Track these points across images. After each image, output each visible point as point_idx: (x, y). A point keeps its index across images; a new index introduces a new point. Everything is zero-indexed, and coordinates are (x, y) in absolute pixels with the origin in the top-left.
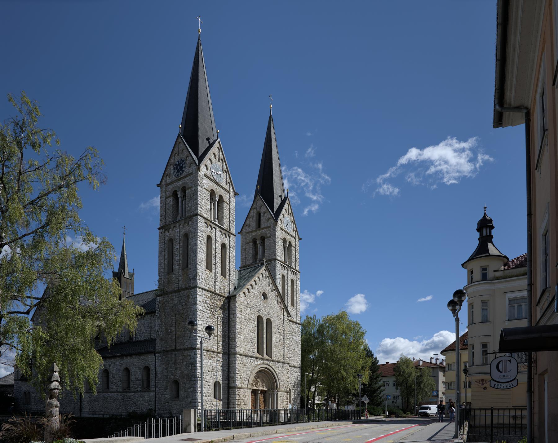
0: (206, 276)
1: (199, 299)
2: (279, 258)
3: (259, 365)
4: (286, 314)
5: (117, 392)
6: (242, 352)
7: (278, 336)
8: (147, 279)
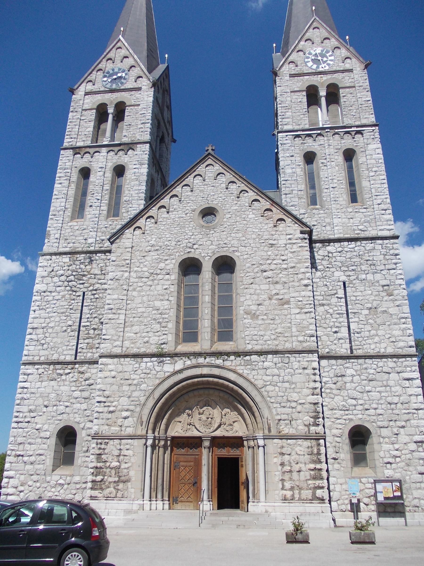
3: (180, 371)
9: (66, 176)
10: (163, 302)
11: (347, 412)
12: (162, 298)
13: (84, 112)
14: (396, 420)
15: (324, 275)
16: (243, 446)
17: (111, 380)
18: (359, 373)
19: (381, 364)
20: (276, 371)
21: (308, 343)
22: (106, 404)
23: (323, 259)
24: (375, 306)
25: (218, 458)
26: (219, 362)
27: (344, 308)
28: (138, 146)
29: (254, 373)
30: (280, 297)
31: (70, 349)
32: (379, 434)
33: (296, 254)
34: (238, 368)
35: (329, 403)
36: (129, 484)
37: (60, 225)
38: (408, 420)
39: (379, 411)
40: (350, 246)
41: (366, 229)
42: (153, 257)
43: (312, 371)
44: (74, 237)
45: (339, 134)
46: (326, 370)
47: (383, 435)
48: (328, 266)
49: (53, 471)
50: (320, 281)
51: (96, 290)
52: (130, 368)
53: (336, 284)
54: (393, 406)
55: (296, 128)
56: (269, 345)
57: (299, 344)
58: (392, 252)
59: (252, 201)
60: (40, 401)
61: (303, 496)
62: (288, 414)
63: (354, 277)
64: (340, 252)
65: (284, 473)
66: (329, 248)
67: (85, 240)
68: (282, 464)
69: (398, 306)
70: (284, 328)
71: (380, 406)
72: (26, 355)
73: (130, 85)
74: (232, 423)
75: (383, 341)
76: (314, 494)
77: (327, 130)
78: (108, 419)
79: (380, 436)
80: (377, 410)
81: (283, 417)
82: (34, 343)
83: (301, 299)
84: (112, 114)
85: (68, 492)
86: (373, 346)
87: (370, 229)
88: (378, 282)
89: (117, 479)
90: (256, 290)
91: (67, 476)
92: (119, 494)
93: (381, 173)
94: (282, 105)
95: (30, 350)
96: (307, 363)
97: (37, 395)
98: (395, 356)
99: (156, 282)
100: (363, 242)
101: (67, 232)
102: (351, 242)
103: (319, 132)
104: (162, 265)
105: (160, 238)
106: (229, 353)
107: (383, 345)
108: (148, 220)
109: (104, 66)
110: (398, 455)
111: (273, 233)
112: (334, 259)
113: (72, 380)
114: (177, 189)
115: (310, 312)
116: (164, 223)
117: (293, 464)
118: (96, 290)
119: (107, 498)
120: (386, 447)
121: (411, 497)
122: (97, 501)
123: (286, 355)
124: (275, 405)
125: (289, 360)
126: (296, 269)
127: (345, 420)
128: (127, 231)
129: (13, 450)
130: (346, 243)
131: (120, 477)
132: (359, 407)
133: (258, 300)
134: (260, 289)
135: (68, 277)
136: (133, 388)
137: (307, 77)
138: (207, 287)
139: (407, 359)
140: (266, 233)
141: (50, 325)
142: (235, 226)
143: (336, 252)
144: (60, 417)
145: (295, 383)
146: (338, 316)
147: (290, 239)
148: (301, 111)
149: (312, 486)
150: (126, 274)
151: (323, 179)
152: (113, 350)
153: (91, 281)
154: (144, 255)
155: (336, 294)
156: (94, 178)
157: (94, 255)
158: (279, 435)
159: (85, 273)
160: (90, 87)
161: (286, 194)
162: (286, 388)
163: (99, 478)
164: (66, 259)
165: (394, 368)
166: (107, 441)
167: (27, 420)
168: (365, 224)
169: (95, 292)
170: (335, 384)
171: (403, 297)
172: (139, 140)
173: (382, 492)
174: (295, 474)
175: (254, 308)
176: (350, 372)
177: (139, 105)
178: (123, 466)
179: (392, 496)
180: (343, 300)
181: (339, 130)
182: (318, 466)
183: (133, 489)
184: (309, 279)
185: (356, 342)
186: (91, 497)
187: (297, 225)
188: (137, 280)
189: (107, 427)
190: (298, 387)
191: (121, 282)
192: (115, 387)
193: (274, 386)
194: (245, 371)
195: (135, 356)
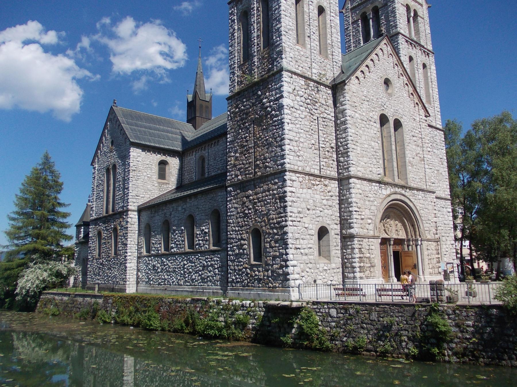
0: (297, 53)
1: (286, 88)
2: (402, 31)
3: (389, 196)
4: (422, 112)
5: (429, 240)
6: (360, 175)
7: (414, 147)
8: (477, 309)
22: (360, 213)
26: (403, 192)
51: (325, 118)
60: (304, 205)
82: (293, 154)
89: (370, 265)
104: (371, 115)
113: (321, 190)
118: (325, 118)
129: (293, 244)
141: (301, 140)
144: (318, 219)
164: (302, 82)
169: (324, 120)
188: (360, 121)
189: (361, 230)
195: (370, 180)
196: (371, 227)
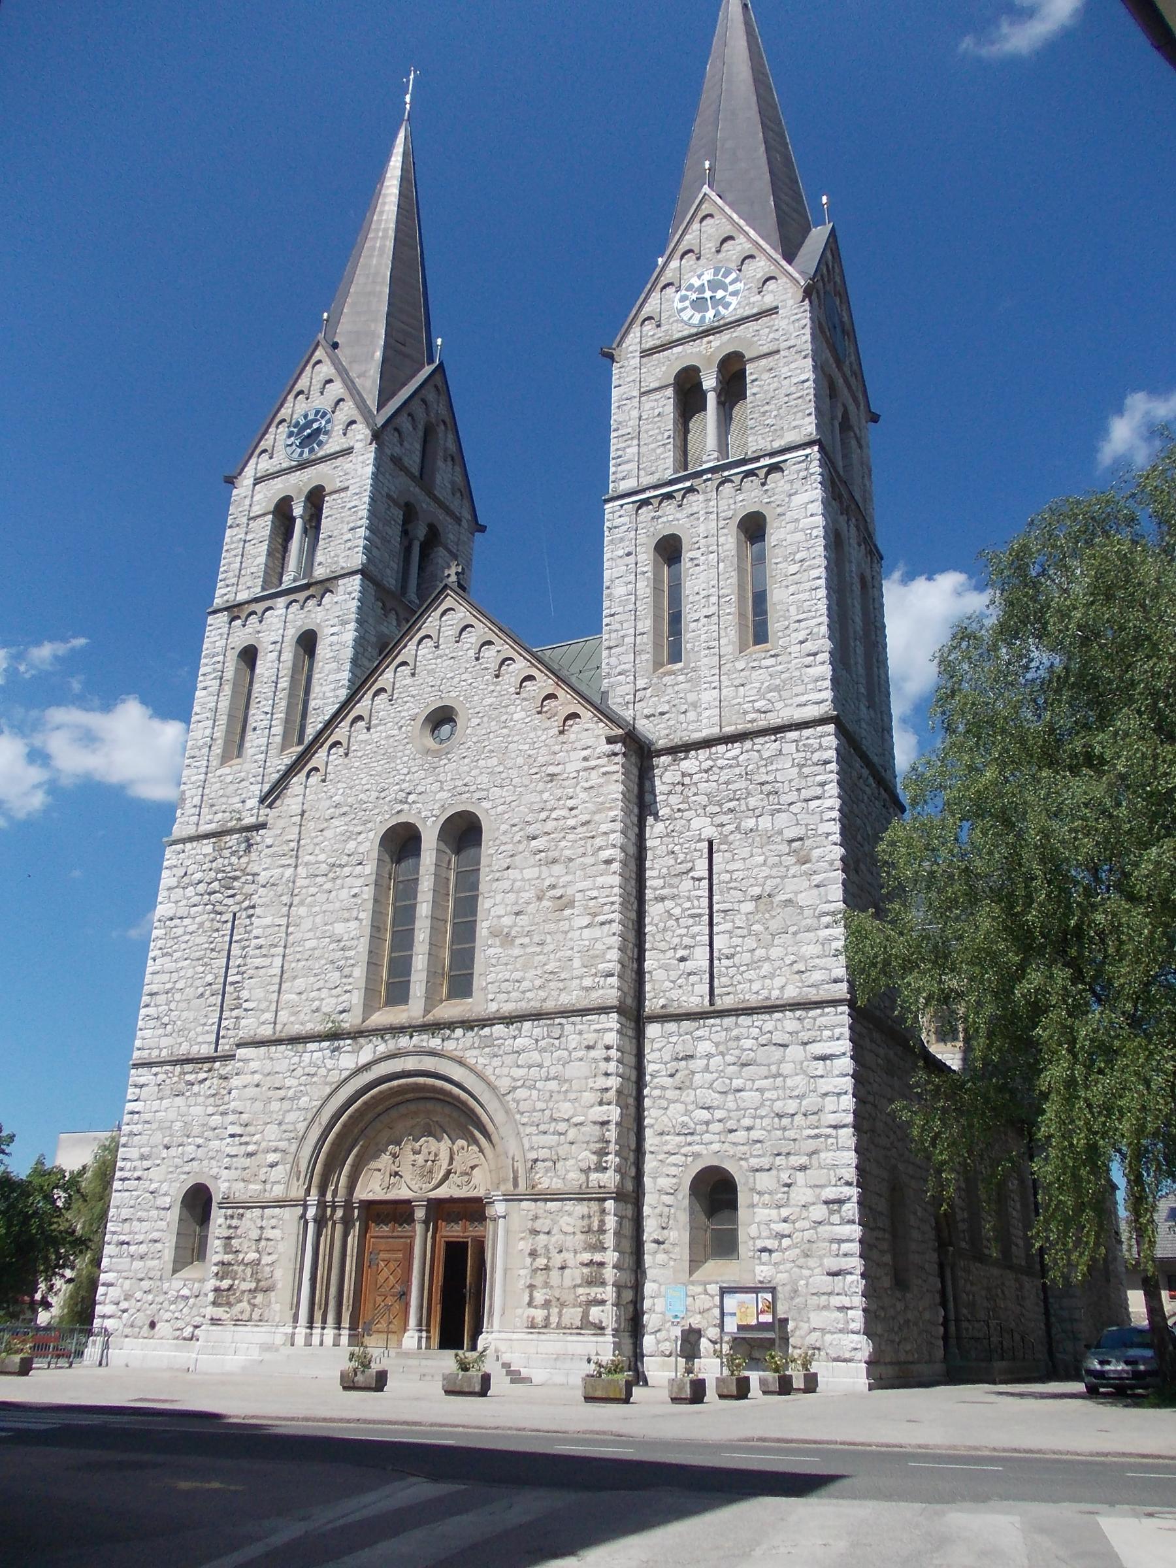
3: (367, 1067)
9: (215, 670)
10: (348, 925)
11: (689, 1139)
12: (346, 915)
13: (252, 524)
14: (788, 1154)
15: (671, 827)
16: (413, 1221)
17: (251, 1091)
18: (721, 1048)
19: (769, 1026)
20: (536, 1056)
21: (601, 992)
22: (244, 1139)
23: (670, 793)
24: (768, 890)
25: (447, 1243)
27: (705, 902)
28: (341, 582)
29: (496, 1062)
30: (557, 892)
31: (208, 1032)
32: (751, 1185)
33: (593, 792)
34: (468, 1054)
35: (657, 1119)
36: (273, 1294)
37: (202, 777)
38: (814, 1153)
39: (755, 1135)
40: (729, 755)
41: (770, 707)
42: (338, 830)
43: (603, 1053)
44: (224, 800)
45: (732, 481)
46: (656, 1046)
47: (758, 1188)
48: (680, 806)
49: (175, 1271)
50: (661, 844)
52: (282, 1066)
53: (693, 846)
54: (786, 1121)
55: (646, 481)
56: (529, 1000)
57: (583, 993)
58: (816, 757)
59: (522, 682)
61: (566, 1321)
62: (550, 1148)
63: (732, 827)
64: (706, 771)
65: (535, 1271)
66: (686, 765)
67: (243, 802)
68: (533, 1254)
69: (817, 886)
70: (560, 960)
71: (758, 1121)
72: (139, 1049)
73: (332, 446)
74: (469, 1170)
75: (778, 972)
76: (585, 1315)
77: (705, 477)
78: (245, 1169)
79: (753, 1190)
80: (752, 1132)
81: (544, 1153)
82: (152, 1023)
83: (595, 893)
84: (301, 517)
85: (195, 1312)
86: (756, 986)
87: (779, 705)
88: (780, 832)
89: (253, 1285)
90: (514, 881)
91: (194, 1280)
92: (257, 1312)
93: (813, 562)
94: (620, 433)
95: (149, 1039)
96: (595, 1035)
97: (155, 1126)
98: (799, 1004)
99: (339, 882)
100: (757, 740)
101: (213, 789)
102: (732, 743)
103: (688, 484)
104: (351, 845)
105: (351, 788)
106: (452, 1023)
107: (778, 982)
108: (333, 750)
109: (290, 411)
110: (786, 1233)
111: (557, 748)
112: (694, 789)
114: (385, 676)
115: (611, 922)
116: (359, 754)
117: (554, 1253)
119: (237, 1322)
120: (762, 1214)
121: (805, 1326)
122: (220, 1328)
123: (557, 1021)
124: (529, 1130)
125: (562, 1030)
126: (591, 827)
127: (686, 1156)
128: (295, 780)
130: (721, 748)
131: (259, 1281)
132: (716, 1127)
133: (516, 903)
134: (523, 880)
135: (209, 884)
136: (287, 1105)
137: (679, 349)
138: (426, 884)
139: (826, 1010)
140: (543, 751)
142: (487, 743)
143: (700, 772)
145: (570, 1081)
146: (691, 921)
147: (585, 759)
148: (659, 437)
149: (583, 1298)
150: (289, 872)
151: (691, 599)
152: (258, 1031)
153: (249, 889)
154: (322, 827)
155: (691, 870)
156: (265, 667)
157: (254, 833)
158: (533, 1192)
159: (238, 873)
160: (263, 464)
161: (610, 648)
162: (552, 1092)
163: (225, 1284)
164: (207, 847)
165: (797, 1033)
166: (241, 1211)
167: (136, 1174)
168: (769, 696)
170: (672, 1076)
171: (831, 863)
172: (342, 568)
173: (734, 1314)
174: (555, 1273)
175: (507, 921)
176: (705, 1047)
177: (346, 488)
178: (266, 1259)
179: (754, 1322)
180: (705, 883)
181: (732, 472)
182: (598, 1257)
183: (278, 1303)
184: (615, 846)
185: (722, 979)
186: (212, 1319)
187: (601, 725)
189: (242, 1185)
190: (574, 1088)
191: (280, 889)
192: (259, 1105)
193: (530, 1088)
194: (481, 1060)
195: (294, 1040)
196: (280, 1172)
